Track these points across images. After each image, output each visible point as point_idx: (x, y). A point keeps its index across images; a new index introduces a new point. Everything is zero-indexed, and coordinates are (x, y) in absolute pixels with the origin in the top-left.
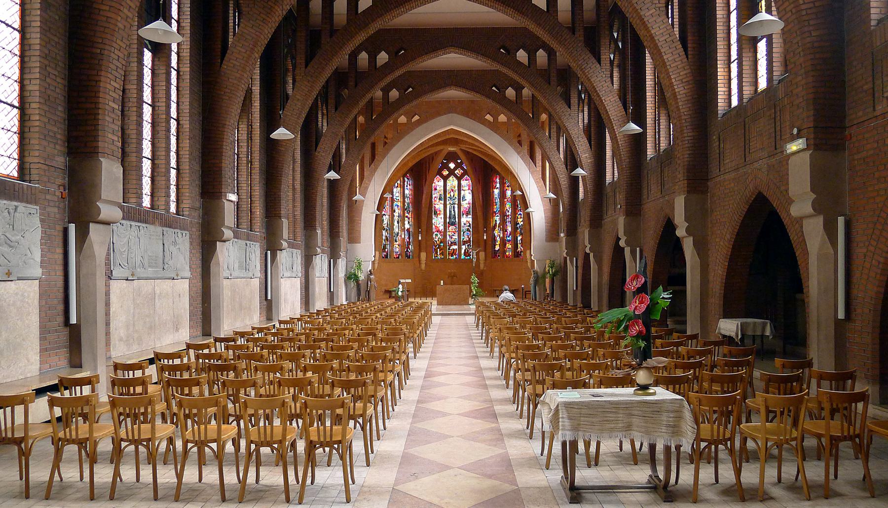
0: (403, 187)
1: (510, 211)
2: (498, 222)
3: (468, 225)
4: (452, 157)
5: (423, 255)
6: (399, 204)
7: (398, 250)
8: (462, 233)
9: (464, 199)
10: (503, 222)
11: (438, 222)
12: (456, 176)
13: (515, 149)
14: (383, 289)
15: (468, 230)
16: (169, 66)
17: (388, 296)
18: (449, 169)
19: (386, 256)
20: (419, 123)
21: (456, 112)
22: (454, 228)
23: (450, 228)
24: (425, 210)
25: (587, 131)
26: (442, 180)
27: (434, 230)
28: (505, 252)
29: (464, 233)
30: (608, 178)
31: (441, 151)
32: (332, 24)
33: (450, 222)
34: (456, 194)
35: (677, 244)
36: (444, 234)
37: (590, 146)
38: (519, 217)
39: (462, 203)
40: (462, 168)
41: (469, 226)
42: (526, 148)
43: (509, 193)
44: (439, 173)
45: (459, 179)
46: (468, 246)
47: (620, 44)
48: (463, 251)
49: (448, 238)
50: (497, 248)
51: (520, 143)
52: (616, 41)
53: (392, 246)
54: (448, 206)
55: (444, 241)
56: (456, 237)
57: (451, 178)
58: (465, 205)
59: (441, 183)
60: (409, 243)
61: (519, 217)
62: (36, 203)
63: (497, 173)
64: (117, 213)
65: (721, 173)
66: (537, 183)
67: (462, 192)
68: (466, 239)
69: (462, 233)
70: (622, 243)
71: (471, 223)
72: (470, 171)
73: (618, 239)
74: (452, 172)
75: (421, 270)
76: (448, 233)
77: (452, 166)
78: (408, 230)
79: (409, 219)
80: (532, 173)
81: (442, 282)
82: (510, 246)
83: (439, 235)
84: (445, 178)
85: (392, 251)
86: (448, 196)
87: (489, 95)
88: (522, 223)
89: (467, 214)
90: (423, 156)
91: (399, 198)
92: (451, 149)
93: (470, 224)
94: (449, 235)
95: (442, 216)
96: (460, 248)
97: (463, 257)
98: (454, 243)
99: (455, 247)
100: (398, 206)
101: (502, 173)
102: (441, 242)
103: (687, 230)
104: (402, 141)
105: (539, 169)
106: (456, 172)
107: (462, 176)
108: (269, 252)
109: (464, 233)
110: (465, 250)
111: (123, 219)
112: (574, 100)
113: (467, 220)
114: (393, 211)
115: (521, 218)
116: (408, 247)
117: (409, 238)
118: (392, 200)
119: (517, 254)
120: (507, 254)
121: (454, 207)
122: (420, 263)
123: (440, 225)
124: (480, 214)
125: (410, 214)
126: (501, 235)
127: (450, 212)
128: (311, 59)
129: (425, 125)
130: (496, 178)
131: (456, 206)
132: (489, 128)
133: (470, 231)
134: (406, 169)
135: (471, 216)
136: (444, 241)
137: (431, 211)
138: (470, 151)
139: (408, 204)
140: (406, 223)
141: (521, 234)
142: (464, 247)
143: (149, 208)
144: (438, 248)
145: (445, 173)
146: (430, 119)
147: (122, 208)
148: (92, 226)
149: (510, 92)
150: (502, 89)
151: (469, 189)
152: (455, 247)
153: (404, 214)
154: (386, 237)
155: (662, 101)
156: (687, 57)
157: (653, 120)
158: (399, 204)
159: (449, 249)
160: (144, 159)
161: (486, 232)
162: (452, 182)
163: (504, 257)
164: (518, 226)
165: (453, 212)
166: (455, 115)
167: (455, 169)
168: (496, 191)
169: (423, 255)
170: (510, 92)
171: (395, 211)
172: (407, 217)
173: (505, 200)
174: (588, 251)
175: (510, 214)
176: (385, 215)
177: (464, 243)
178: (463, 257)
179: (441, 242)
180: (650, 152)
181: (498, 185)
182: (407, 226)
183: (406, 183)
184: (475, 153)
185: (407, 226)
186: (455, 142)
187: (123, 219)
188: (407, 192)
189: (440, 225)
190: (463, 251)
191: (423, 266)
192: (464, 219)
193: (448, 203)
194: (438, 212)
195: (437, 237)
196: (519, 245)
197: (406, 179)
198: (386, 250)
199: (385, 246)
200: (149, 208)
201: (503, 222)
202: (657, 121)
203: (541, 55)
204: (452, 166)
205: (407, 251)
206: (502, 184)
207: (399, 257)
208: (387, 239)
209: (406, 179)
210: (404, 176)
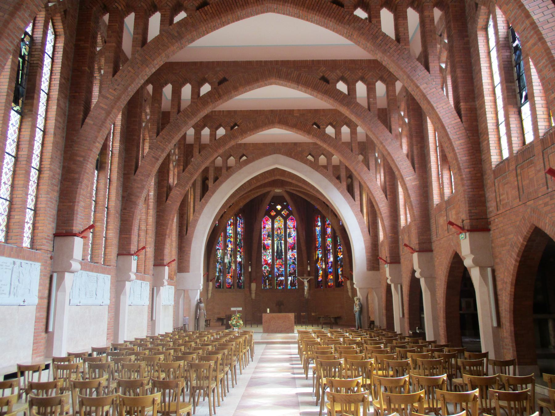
0: (235, 224)
1: (331, 246)
2: (320, 256)
3: (294, 258)
4: (278, 199)
5: (253, 286)
6: (232, 240)
7: (230, 281)
8: (288, 266)
9: (290, 236)
10: (325, 255)
11: (267, 257)
12: (282, 216)
13: (335, 185)
14: (217, 316)
15: (294, 263)
16: (34, 126)
17: (221, 323)
18: (276, 210)
19: (219, 287)
20: (246, 163)
21: (280, 153)
22: (281, 261)
23: (278, 261)
24: (255, 246)
25: (410, 156)
26: (270, 220)
27: (263, 263)
28: (327, 282)
29: (290, 265)
30: (403, 222)
31: (268, 192)
32: (200, 142)
33: (278, 255)
34: (283, 231)
35: (465, 272)
36: (272, 266)
37: (414, 168)
38: (339, 251)
39: (288, 239)
40: (288, 210)
41: (295, 259)
42: (344, 185)
43: (329, 230)
44: (268, 213)
45: (285, 219)
46: (294, 277)
47: (406, 120)
48: (289, 282)
49: (276, 270)
50: (320, 279)
51: (338, 178)
52: (403, 118)
53: (225, 277)
54: (276, 242)
55: (271, 272)
56: (282, 269)
57: (278, 218)
58: (290, 241)
59: (269, 222)
60: (240, 274)
61: (339, 251)
62: (109, 274)
63: (319, 212)
64: (79, 266)
65: (499, 212)
66: (356, 215)
67: (288, 231)
68: (292, 271)
69: (288, 266)
70: (417, 275)
71: (296, 256)
72: (295, 212)
73: (414, 272)
74: (279, 213)
75: (252, 299)
76: (276, 266)
77: (279, 207)
78: (240, 263)
79: (241, 253)
80: (351, 207)
81: (268, 310)
82: (332, 277)
83: (268, 268)
84: (273, 218)
85: (224, 281)
86: (275, 233)
87: (306, 162)
88: (342, 256)
89: (293, 249)
90: (253, 197)
91: (232, 235)
92: (278, 191)
93: (295, 258)
94: (277, 268)
95: (271, 251)
96: (286, 280)
97: (289, 287)
98: (280, 275)
99: (283, 278)
100: (230, 242)
101: (324, 212)
102: (269, 274)
103: (474, 261)
104: (230, 178)
105: (358, 202)
106: (282, 213)
107: (288, 216)
108: (155, 288)
109: (290, 265)
110: (291, 281)
111: (81, 269)
112: (372, 163)
113: (292, 255)
114: (226, 246)
115: (341, 251)
116: (240, 279)
117: (241, 270)
118: (226, 237)
119: (339, 285)
120: (329, 284)
121: (281, 243)
122: (251, 293)
123: (269, 258)
124: (304, 248)
125: (242, 249)
126: (324, 267)
127: (278, 247)
128: (162, 129)
129: (251, 165)
130: (318, 217)
131: (283, 242)
132: (310, 166)
133: (295, 264)
134: (237, 209)
135: (296, 251)
136: (271, 272)
137: (261, 247)
138: (294, 192)
139: (240, 240)
140: (238, 256)
141: (341, 266)
142: (290, 278)
143: (29, 248)
144: (267, 279)
145: (273, 213)
146: (257, 159)
147: (81, 263)
148: (67, 275)
149: (322, 160)
150: (316, 158)
151: (294, 227)
152: (283, 278)
153: (236, 248)
154: (220, 269)
155: (444, 159)
156: (387, 199)
157: (495, 124)
158: (232, 240)
159: (277, 280)
160: (28, 210)
161: (309, 264)
162: (279, 223)
163: (326, 287)
164: (338, 259)
165: (280, 247)
166: (280, 156)
167: (282, 210)
168: (318, 229)
169: (253, 286)
170: (322, 160)
171: (228, 246)
172: (239, 251)
173: (326, 236)
174: (389, 282)
175: (330, 248)
176: (218, 249)
177: (291, 275)
178: (289, 287)
179: (269, 274)
180: (436, 199)
181: (319, 224)
182: (239, 259)
183: (238, 222)
184: (298, 194)
185: (239, 259)
186: (281, 183)
187: (81, 269)
188: (239, 229)
189: (269, 258)
190: (289, 282)
191: (253, 296)
192: (290, 254)
193: (275, 239)
194: (267, 248)
195: (266, 269)
196: (340, 276)
197: (238, 218)
198: (220, 281)
199: (218, 277)
200: (29, 248)
201: (325, 255)
202: (440, 177)
203: (345, 130)
204: (279, 207)
205: (239, 281)
206: (323, 222)
207: (230, 288)
208: (220, 271)
209: (238, 218)
210: (236, 215)
